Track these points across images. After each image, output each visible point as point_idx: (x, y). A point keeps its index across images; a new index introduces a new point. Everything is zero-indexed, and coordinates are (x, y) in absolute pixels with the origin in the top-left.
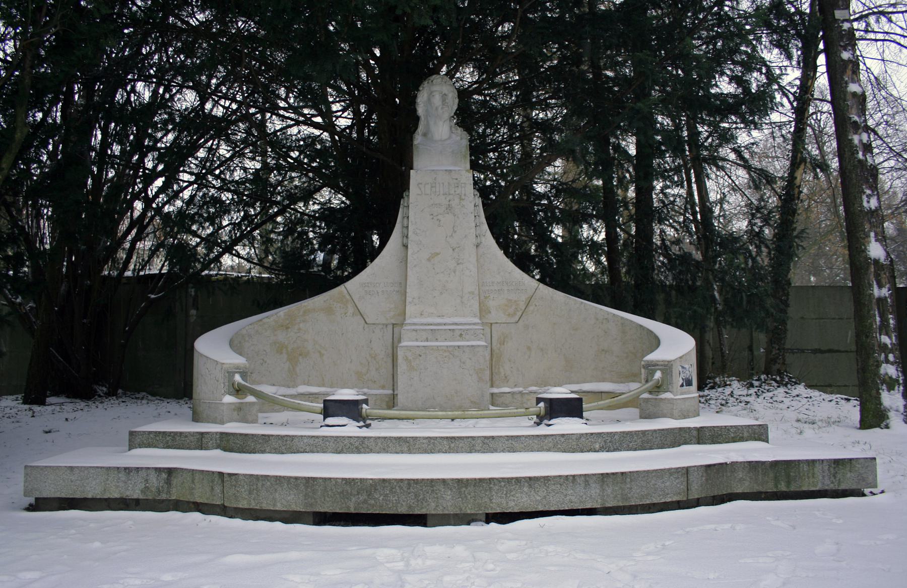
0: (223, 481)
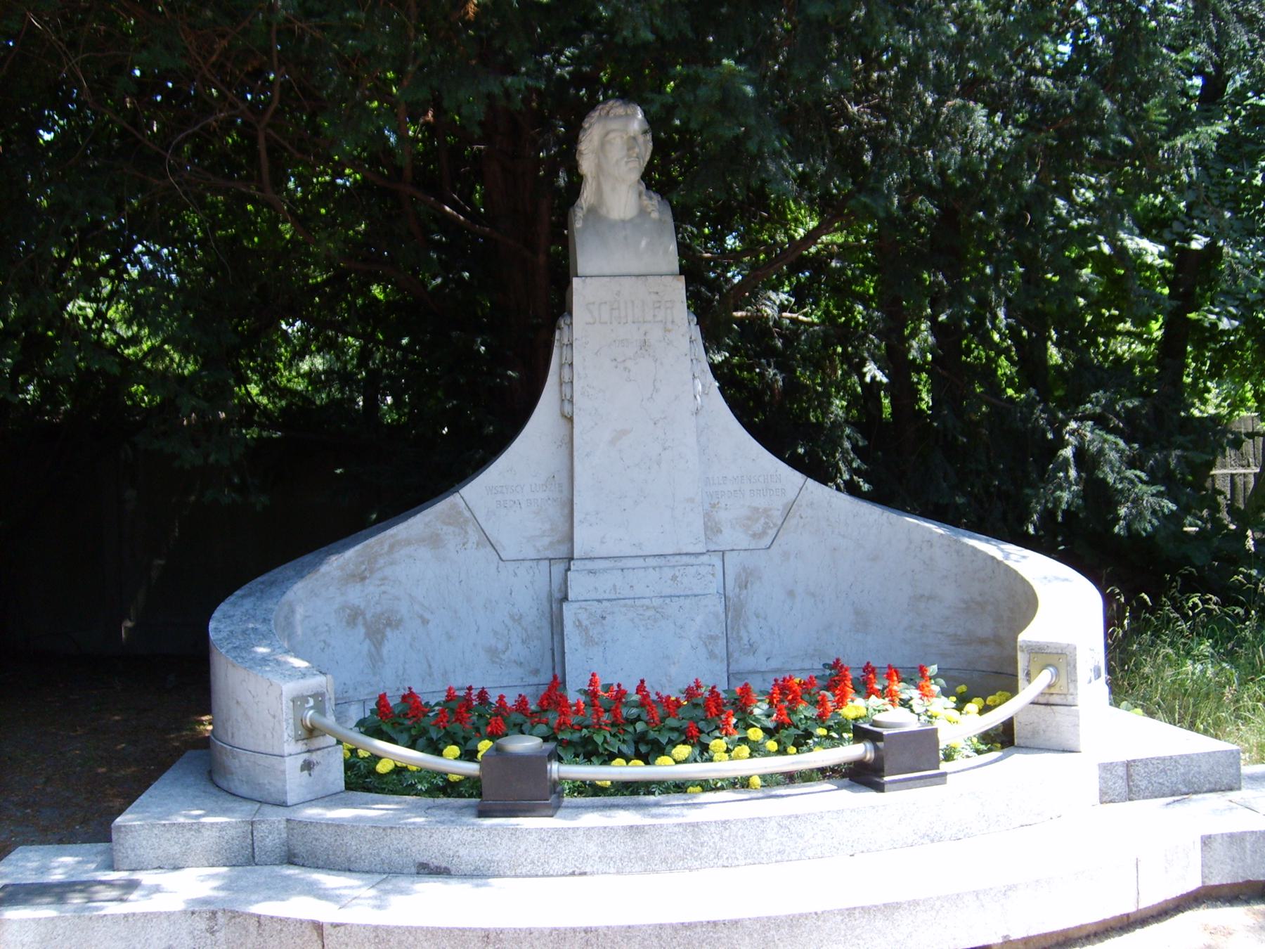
0: (321, 936)
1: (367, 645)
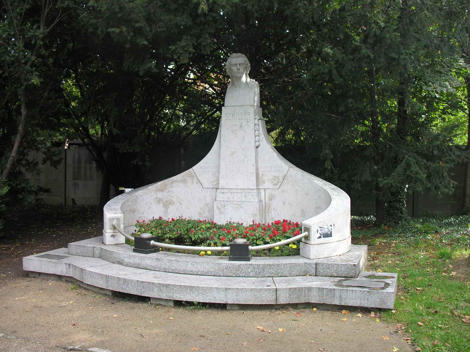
1: (163, 209)
